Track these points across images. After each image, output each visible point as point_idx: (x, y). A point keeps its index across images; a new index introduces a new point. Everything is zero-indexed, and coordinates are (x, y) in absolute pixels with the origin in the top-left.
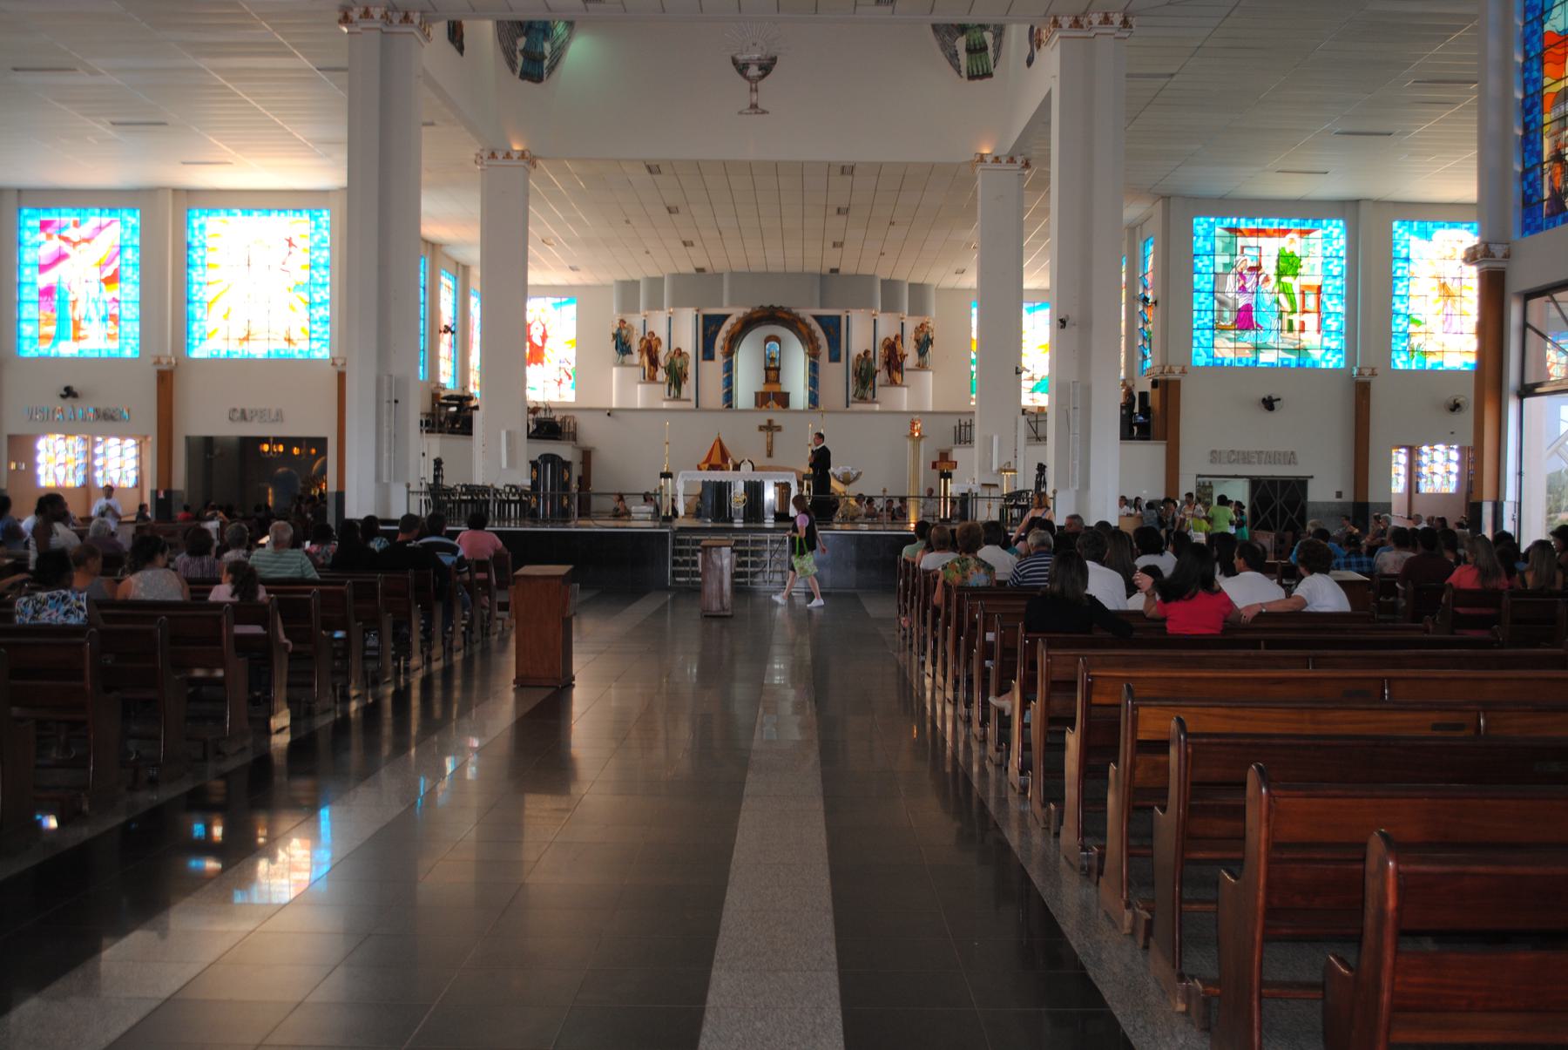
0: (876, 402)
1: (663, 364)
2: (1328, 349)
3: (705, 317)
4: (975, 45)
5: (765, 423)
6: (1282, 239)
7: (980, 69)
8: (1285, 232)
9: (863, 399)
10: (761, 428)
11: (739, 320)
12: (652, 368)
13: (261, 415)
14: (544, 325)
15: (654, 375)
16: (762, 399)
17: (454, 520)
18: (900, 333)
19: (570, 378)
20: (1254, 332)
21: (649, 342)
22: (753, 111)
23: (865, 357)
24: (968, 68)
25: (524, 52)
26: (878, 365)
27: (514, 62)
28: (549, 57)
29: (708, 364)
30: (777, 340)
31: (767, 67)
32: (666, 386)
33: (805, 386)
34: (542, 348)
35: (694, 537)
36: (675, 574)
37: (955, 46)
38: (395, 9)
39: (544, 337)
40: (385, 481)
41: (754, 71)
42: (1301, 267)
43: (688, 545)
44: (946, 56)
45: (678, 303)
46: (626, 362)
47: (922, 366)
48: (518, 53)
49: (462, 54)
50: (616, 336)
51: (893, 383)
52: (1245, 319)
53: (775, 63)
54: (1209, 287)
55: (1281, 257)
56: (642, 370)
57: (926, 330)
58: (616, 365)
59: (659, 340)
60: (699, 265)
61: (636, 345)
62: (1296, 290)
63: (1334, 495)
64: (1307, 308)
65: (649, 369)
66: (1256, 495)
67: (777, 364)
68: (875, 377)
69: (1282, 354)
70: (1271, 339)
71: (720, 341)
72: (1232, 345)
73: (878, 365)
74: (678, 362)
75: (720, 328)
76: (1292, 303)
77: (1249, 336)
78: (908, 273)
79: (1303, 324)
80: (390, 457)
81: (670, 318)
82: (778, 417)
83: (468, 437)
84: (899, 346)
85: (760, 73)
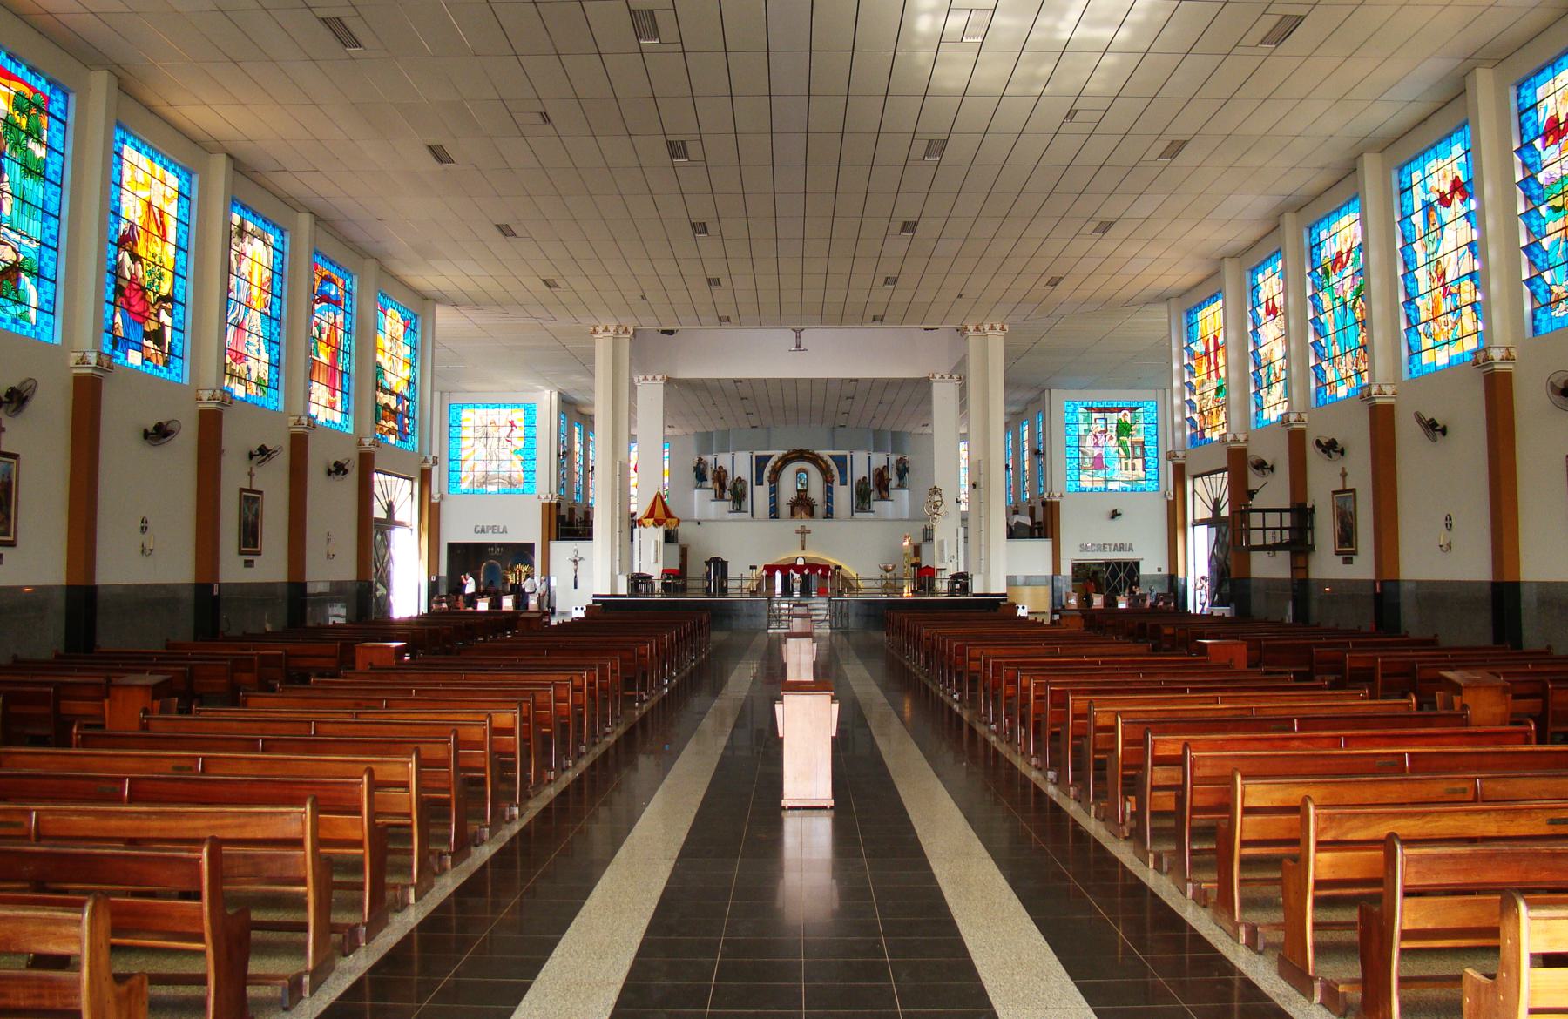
2: (1150, 480)
8: (1120, 410)
9: (863, 510)
10: (797, 532)
13: (493, 529)
18: (886, 464)
20: (1104, 471)
30: (804, 471)
36: (485, 721)
38: (621, 326)
50: (697, 469)
52: (1098, 463)
54: (1076, 444)
59: (725, 471)
62: (1129, 444)
69: (1122, 484)
70: (1115, 475)
72: (1091, 479)
74: (739, 487)
77: (1101, 473)
79: (1133, 465)
81: (733, 458)
84: (885, 474)
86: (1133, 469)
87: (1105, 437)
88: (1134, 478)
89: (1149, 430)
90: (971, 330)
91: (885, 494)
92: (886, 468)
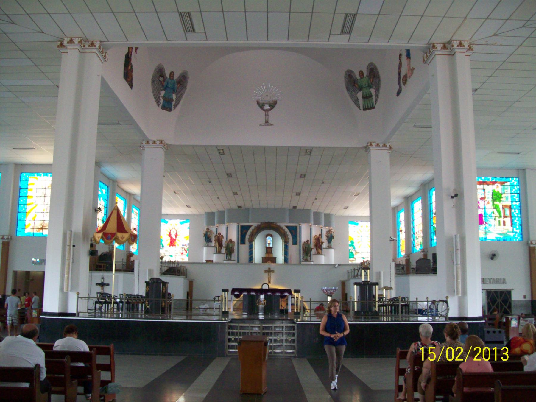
0: (312, 261)
1: (224, 246)
2: (516, 233)
3: (242, 227)
4: (366, 95)
5: (267, 269)
6: (493, 186)
7: (369, 105)
8: (494, 183)
9: (306, 260)
10: (266, 271)
11: (255, 227)
12: (220, 247)
14: (176, 230)
15: (221, 251)
16: (265, 260)
17: (108, 313)
18: (321, 233)
19: (186, 252)
21: (219, 237)
22: (266, 124)
23: (307, 243)
24: (363, 105)
25: (164, 97)
26: (312, 246)
27: (159, 101)
28: (175, 100)
29: (242, 245)
31: (273, 105)
32: (225, 255)
33: (283, 255)
34: (175, 240)
35: (240, 325)
37: (357, 96)
38: (87, 40)
39: (176, 235)
40: (65, 291)
41: (267, 107)
42: (502, 198)
43: (240, 333)
44: (353, 101)
45: (231, 221)
46: (209, 245)
47: (329, 247)
48: (161, 98)
49: (132, 88)
51: (318, 254)
53: (277, 103)
55: (493, 193)
56: (215, 248)
57: (331, 232)
58: (205, 246)
59: (222, 236)
60: (239, 205)
61: (213, 239)
62: (501, 207)
63: (523, 297)
64: (506, 215)
65: (219, 248)
66: (490, 298)
67: (271, 246)
68: (311, 251)
71: (247, 237)
73: (312, 246)
74: (230, 245)
75: (247, 231)
76: (499, 213)
78: (324, 209)
79: (504, 222)
80: (68, 278)
81: (227, 227)
82: (272, 266)
83: (132, 273)
84: (320, 239)
85: (269, 108)
86: (504, 225)
87: (484, 201)
88: (505, 231)
89: (515, 197)
90: (439, 48)
91: (320, 251)
92: (321, 235)
